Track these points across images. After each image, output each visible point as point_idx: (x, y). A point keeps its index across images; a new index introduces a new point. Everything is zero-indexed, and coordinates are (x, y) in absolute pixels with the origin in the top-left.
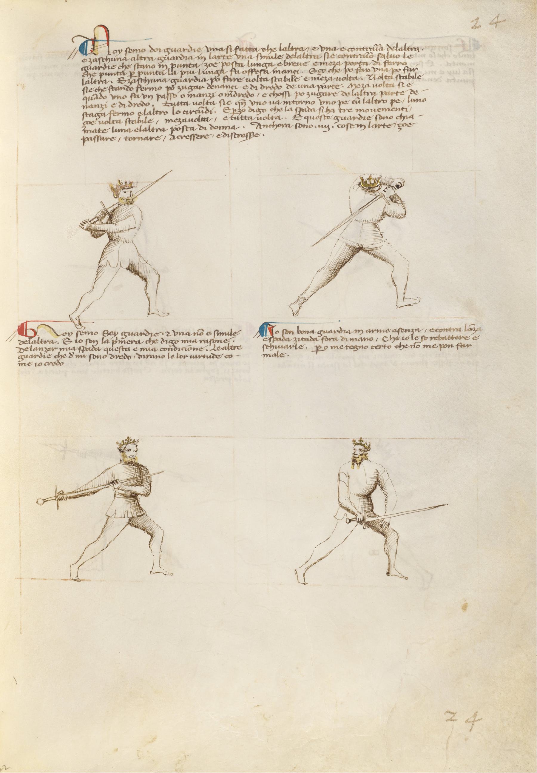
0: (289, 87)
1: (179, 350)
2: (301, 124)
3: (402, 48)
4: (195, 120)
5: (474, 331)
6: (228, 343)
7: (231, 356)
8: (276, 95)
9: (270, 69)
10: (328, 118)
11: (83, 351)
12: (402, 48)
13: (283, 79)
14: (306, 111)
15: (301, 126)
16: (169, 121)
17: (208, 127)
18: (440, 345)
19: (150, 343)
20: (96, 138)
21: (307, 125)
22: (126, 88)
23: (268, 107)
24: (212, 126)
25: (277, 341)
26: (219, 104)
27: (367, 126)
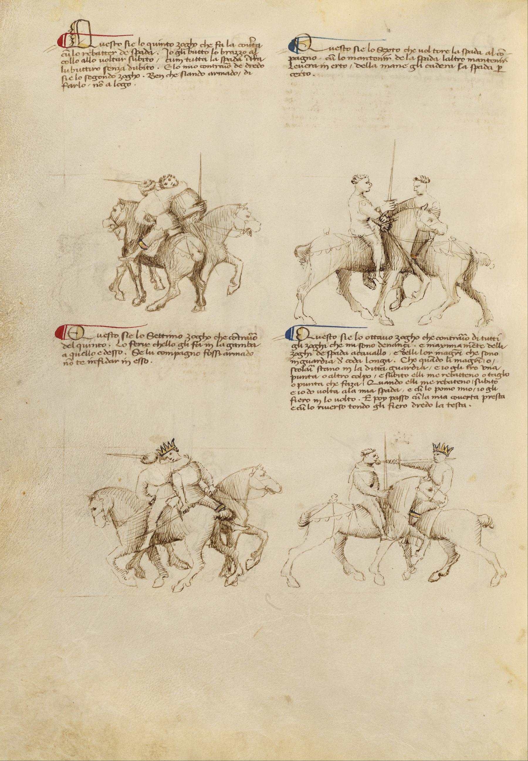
1: (134, 69)
3: (332, 375)
4: (425, 51)
5: (119, 71)
6: (170, 71)
7: (335, 337)
12: (332, 375)
13: (70, 70)
15: (364, 346)
18: (124, 70)
21: (77, 71)
26: (327, 354)
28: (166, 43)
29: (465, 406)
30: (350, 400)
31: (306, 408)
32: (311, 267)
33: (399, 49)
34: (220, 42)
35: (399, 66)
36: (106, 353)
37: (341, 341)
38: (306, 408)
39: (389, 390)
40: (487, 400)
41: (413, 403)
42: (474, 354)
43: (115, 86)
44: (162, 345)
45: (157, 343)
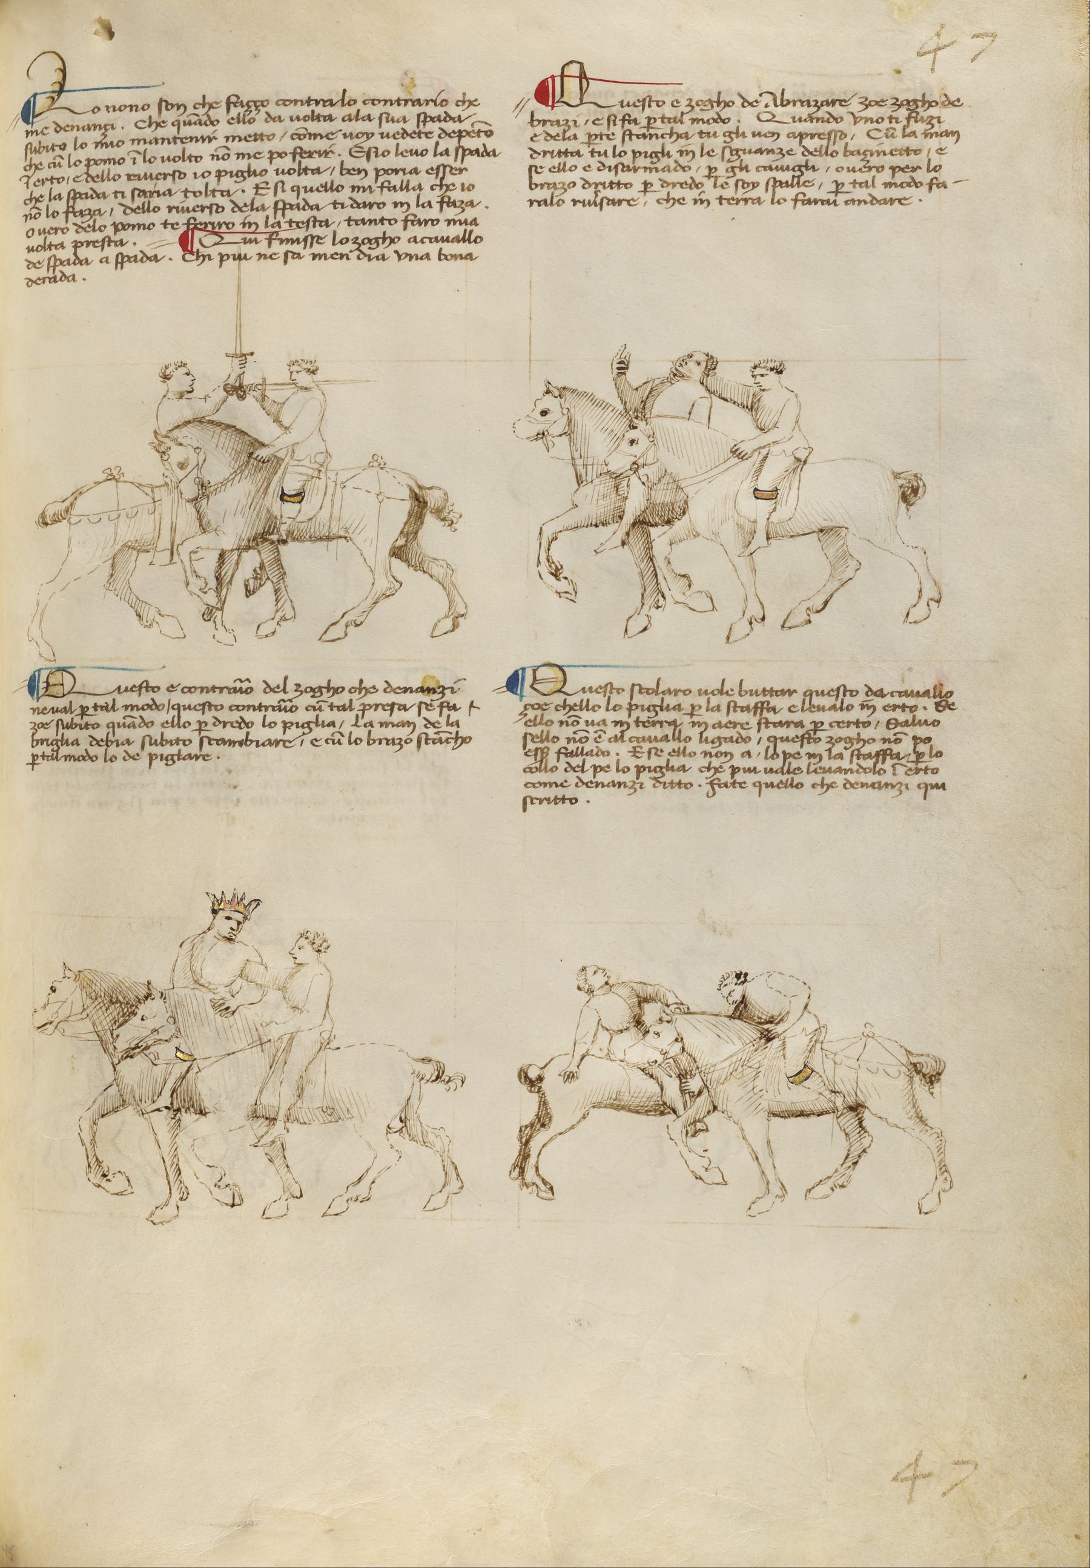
0: (80, 230)
2: (746, 181)
8: (467, 104)
9: (162, 202)
10: (885, 740)
11: (425, 122)
14: (135, 261)
16: (139, 141)
17: (229, 206)
19: (441, 189)
20: (441, 169)
22: (89, 195)
23: (342, 145)
24: (268, 686)
25: (434, 122)
27: (698, 153)
28: (305, 99)
29: (238, 155)
30: (386, 222)
31: (345, 741)
32: (738, 124)
33: (274, 135)
34: (630, 116)
35: (237, 139)
36: (848, 786)
37: (703, 144)
38: (345, 741)
39: (86, 194)
40: (156, 763)
41: (531, 149)
42: (679, 136)
43: (69, 166)
44: (571, 708)
45: (562, 703)
